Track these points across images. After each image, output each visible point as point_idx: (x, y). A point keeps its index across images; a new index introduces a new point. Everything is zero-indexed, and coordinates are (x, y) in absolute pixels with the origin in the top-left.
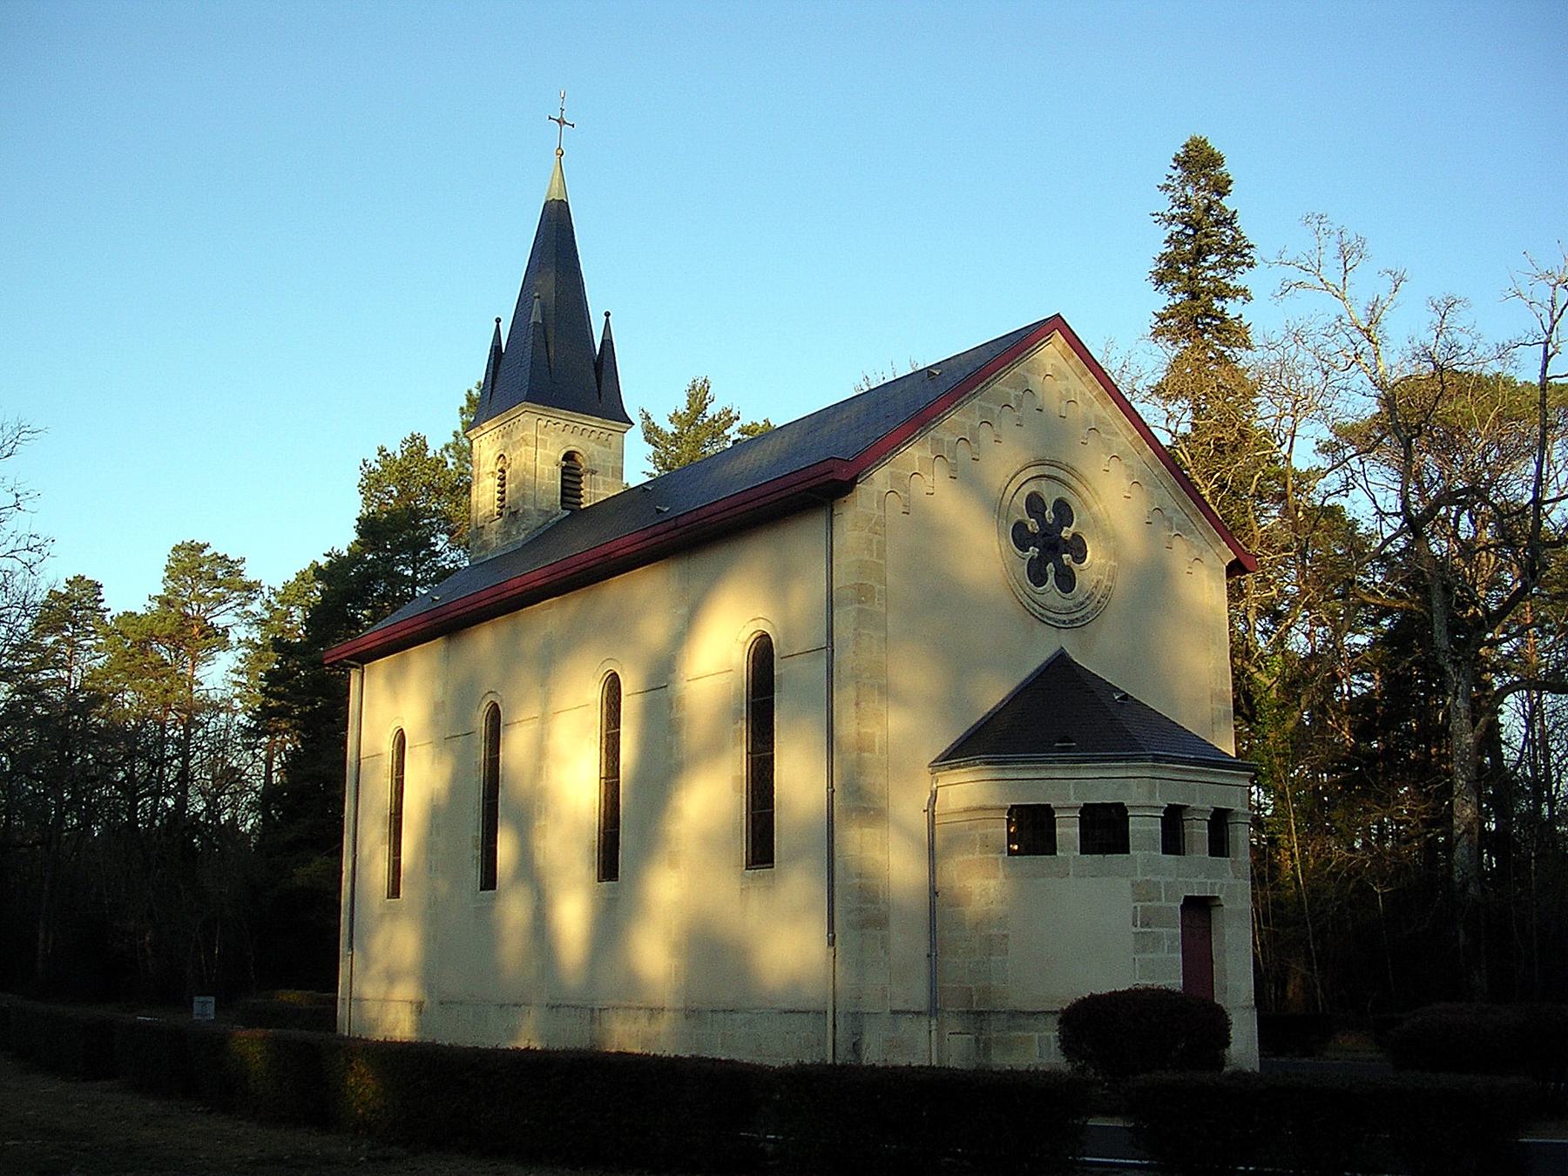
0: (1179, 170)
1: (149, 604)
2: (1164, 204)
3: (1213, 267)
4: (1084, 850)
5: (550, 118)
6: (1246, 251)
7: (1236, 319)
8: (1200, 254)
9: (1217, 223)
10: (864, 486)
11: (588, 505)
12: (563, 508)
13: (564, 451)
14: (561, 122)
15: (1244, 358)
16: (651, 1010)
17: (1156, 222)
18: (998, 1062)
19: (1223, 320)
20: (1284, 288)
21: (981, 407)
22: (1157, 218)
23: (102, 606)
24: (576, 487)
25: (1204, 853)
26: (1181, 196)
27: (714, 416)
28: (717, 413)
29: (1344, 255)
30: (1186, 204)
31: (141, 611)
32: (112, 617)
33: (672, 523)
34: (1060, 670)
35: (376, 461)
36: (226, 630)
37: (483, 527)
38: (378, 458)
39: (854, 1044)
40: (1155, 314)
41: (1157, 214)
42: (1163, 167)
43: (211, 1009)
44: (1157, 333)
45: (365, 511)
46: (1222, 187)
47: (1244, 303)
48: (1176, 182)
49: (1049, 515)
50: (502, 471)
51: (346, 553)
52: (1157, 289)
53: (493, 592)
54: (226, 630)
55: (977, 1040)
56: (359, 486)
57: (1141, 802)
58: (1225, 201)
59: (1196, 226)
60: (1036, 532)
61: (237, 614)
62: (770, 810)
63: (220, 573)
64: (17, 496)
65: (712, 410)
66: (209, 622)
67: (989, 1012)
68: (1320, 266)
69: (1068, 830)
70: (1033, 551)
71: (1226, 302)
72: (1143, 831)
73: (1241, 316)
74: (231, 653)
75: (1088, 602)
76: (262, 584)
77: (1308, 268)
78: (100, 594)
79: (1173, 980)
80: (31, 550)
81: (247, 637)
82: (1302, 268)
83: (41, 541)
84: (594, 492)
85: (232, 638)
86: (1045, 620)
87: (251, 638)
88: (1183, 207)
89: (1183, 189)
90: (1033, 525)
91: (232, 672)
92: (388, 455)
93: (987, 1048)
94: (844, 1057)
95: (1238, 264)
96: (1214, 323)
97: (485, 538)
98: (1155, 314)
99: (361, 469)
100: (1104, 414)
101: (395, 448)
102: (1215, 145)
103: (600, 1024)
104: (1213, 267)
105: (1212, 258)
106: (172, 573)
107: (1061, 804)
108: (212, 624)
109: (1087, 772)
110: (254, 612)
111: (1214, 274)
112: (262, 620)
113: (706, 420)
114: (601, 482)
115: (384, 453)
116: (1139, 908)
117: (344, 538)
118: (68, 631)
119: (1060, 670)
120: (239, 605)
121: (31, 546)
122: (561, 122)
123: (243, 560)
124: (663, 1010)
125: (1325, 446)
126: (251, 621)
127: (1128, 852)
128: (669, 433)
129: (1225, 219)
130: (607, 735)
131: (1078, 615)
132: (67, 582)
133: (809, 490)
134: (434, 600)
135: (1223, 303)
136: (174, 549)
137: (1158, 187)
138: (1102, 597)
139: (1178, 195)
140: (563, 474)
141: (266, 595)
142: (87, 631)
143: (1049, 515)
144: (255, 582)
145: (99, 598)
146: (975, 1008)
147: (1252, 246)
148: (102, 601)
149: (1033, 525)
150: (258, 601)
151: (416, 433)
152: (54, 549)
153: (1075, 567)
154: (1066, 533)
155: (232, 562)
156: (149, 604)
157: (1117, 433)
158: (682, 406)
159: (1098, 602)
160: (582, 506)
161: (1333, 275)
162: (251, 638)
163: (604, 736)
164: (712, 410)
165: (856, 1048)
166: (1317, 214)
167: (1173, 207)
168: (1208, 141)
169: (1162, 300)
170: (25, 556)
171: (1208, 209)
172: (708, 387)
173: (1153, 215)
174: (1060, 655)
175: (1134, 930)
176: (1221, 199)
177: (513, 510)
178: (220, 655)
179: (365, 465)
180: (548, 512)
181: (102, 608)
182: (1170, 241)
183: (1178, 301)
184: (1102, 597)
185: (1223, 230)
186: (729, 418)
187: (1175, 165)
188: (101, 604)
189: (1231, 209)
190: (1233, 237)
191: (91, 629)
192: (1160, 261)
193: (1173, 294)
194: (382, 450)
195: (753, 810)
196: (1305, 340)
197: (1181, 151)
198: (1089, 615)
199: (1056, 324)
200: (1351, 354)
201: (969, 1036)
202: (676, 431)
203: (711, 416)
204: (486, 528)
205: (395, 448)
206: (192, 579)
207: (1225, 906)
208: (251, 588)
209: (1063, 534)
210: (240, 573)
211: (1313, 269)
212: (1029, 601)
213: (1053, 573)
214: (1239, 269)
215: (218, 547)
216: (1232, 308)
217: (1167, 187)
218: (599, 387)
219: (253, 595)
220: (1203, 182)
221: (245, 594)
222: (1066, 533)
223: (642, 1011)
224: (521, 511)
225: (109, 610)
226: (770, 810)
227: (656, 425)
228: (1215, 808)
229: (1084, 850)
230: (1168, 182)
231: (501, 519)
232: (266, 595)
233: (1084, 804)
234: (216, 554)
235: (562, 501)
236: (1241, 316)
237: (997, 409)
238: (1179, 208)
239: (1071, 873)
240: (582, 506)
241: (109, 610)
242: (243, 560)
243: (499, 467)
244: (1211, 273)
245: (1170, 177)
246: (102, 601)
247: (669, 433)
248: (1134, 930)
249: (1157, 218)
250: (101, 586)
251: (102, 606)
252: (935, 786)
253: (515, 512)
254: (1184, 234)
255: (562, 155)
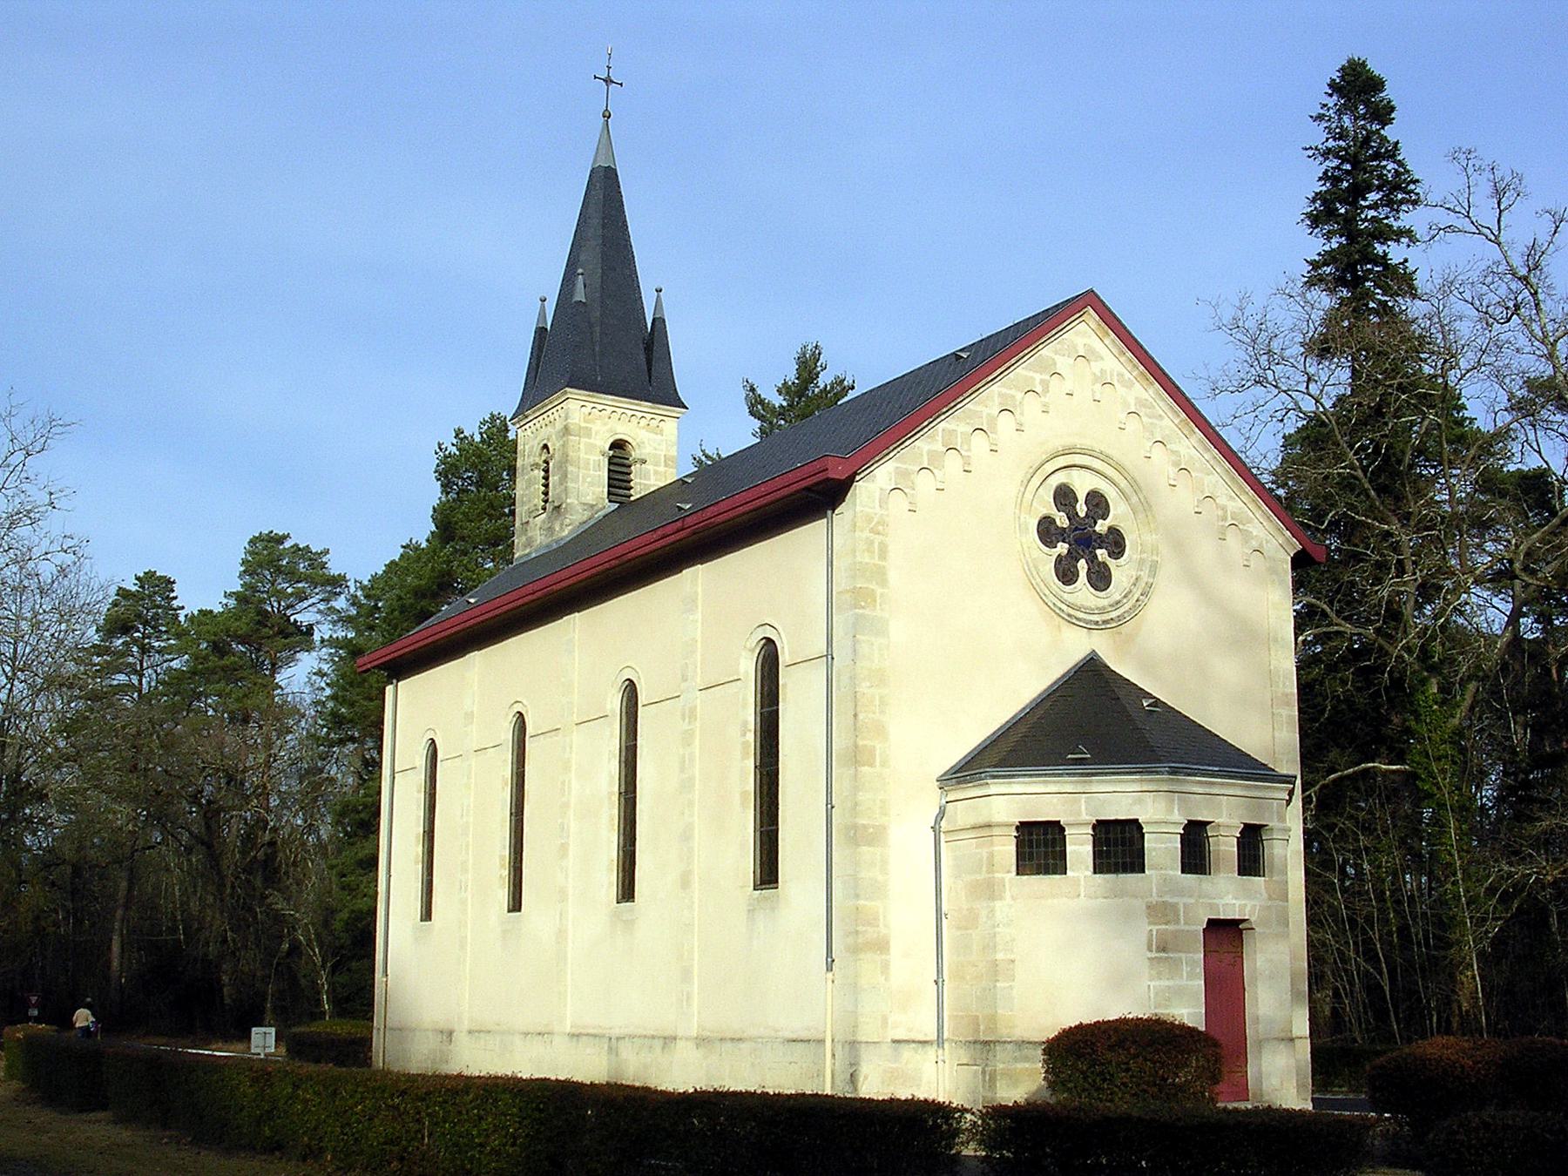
0: (1335, 97)
1: (225, 601)
2: (1318, 136)
3: (1374, 206)
4: (1098, 868)
5: (595, 77)
6: (1412, 187)
7: (1400, 264)
8: (1359, 191)
9: (1377, 156)
10: (865, 484)
11: (638, 496)
12: (610, 501)
13: (611, 440)
14: (608, 81)
15: (1415, 309)
16: (665, 1038)
17: (1309, 157)
18: (1005, 1095)
19: (1386, 266)
20: (1432, 232)
21: (1000, 395)
22: (1310, 153)
23: (175, 603)
24: (625, 478)
25: (1233, 872)
26: (1337, 127)
27: (826, 386)
28: (829, 382)
29: (1499, 193)
30: (1342, 136)
31: (218, 609)
32: (186, 616)
33: (679, 524)
34: (1091, 673)
35: (453, 445)
36: (310, 628)
37: (527, 522)
38: (455, 441)
39: (852, 1075)
40: (1307, 262)
41: (1311, 148)
42: (1318, 95)
43: (272, 1040)
44: (1310, 283)
45: (443, 499)
46: (1383, 114)
47: (1409, 246)
48: (1331, 111)
49: (1082, 509)
50: (546, 462)
51: (424, 545)
52: (1311, 233)
53: (514, 595)
54: (310, 628)
55: (984, 1072)
56: (435, 472)
57: (1157, 817)
58: (1388, 132)
59: (1355, 163)
60: (1065, 526)
61: (319, 611)
62: (774, 828)
63: (302, 565)
64: (51, 494)
65: (824, 380)
66: (292, 619)
67: (994, 1042)
68: (1469, 207)
69: (1079, 848)
70: (1062, 548)
71: (1389, 246)
72: (1160, 848)
73: (1406, 261)
74: (314, 654)
75: (1125, 601)
76: (348, 578)
77: (1457, 209)
78: (173, 591)
79: (1189, 1011)
80: (66, 552)
81: (331, 636)
82: (1449, 209)
83: (75, 541)
84: (648, 479)
85: (317, 637)
86: (1074, 621)
87: (335, 636)
88: (1339, 139)
89: (1340, 119)
90: (1062, 520)
91: (314, 674)
92: (466, 437)
93: (993, 1080)
94: (842, 1090)
95: (1402, 202)
96: (1376, 269)
97: (530, 534)
98: (1307, 262)
99: (436, 453)
100: (1147, 396)
101: (473, 431)
102: (1375, 67)
103: (617, 1055)
104: (1374, 206)
105: (1373, 196)
106: (251, 568)
107: (1071, 819)
108: (296, 621)
109: (1018, 785)
110: (338, 608)
111: (1375, 214)
112: (349, 616)
113: (817, 390)
114: (652, 472)
115: (462, 436)
116: (1154, 933)
117: (422, 530)
118: (139, 631)
119: (1091, 673)
120: (322, 600)
121: (65, 547)
122: (608, 81)
123: (327, 552)
124: (675, 1039)
125: (1519, 403)
126: (335, 618)
127: (1144, 872)
128: (777, 406)
129: (1387, 151)
130: (627, 747)
131: (1114, 615)
132: (137, 579)
133: (808, 489)
134: (469, 603)
135: (1385, 247)
136: (251, 541)
137: (1311, 117)
138: (1142, 595)
139: (1334, 125)
140: (610, 463)
141: (352, 590)
142: (160, 631)
143: (1082, 509)
144: (340, 575)
145: (172, 595)
146: (982, 1038)
147: (1417, 181)
148: (175, 598)
149: (1062, 520)
150: (343, 596)
151: (496, 413)
152: (87, 551)
153: (1111, 563)
154: (1101, 527)
155: (316, 553)
156: (225, 601)
157: (1160, 416)
158: (791, 375)
159: (1137, 601)
160: (632, 499)
161: (1485, 213)
162: (335, 636)
163: (623, 748)
164: (824, 380)
165: (853, 1078)
166: (1464, 150)
167: (1327, 139)
168: (1368, 63)
169: (1316, 245)
170: (60, 558)
171: (1366, 141)
172: (819, 354)
173: (1306, 149)
174: (1092, 658)
175: (1150, 955)
176: (1383, 128)
177: (556, 504)
178: (302, 656)
179: (441, 449)
180: (592, 506)
181: (175, 606)
182: (1325, 177)
183: (1335, 246)
184: (1142, 595)
185: (1384, 163)
186: (841, 388)
187: (1330, 92)
188: (174, 602)
189: (1392, 139)
190: (1396, 171)
191: (164, 629)
192: (1314, 201)
193: (1329, 239)
194: (458, 432)
195: (761, 827)
196: (1461, 290)
197: (1336, 76)
198: (1126, 615)
199: (1089, 301)
200: (1511, 304)
201: (975, 1067)
202: (785, 404)
203: (822, 386)
204: (531, 524)
205: (473, 431)
206: (271, 573)
207: (1257, 929)
208: (338, 582)
209: (1097, 528)
210: (323, 566)
211: (1463, 211)
212: (1055, 600)
213: (1086, 570)
214: (1404, 207)
215: (298, 539)
216: (1395, 252)
217: (1320, 117)
218: (649, 370)
219: (338, 590)
220: (1362, 109)
221: (329, 588)
222: (1101, 527)
223: (656, 1040)
224: (564, 506)
225: (183, 608)
226: (774, 828)
227: (762, 397)
228: (1245, 824)
229: (1098, 868)
230: (1322, 112)
231: (544, 515)
232: (352, 590)
233: (1097, 821)
234: (296, 545)
235: (609, 493)
236: (1406, 261)
237: (1019, 396)
238: (1335, 140)
239: (1082, 895)
240: (632, 499)
241: (183, 608)
242: (327, 552)
243: (543, 458)
244: (1372, 213)
245: (1325, 105)
246: (175, 598)
247: (777, 406)
248: (1150, 955)
249: (1310, 153)
250: (174, 582)
251: (175, 603)
252: (944, 802)
253: (559, 507)
254: (1342, 170)
255: (609, 117)
